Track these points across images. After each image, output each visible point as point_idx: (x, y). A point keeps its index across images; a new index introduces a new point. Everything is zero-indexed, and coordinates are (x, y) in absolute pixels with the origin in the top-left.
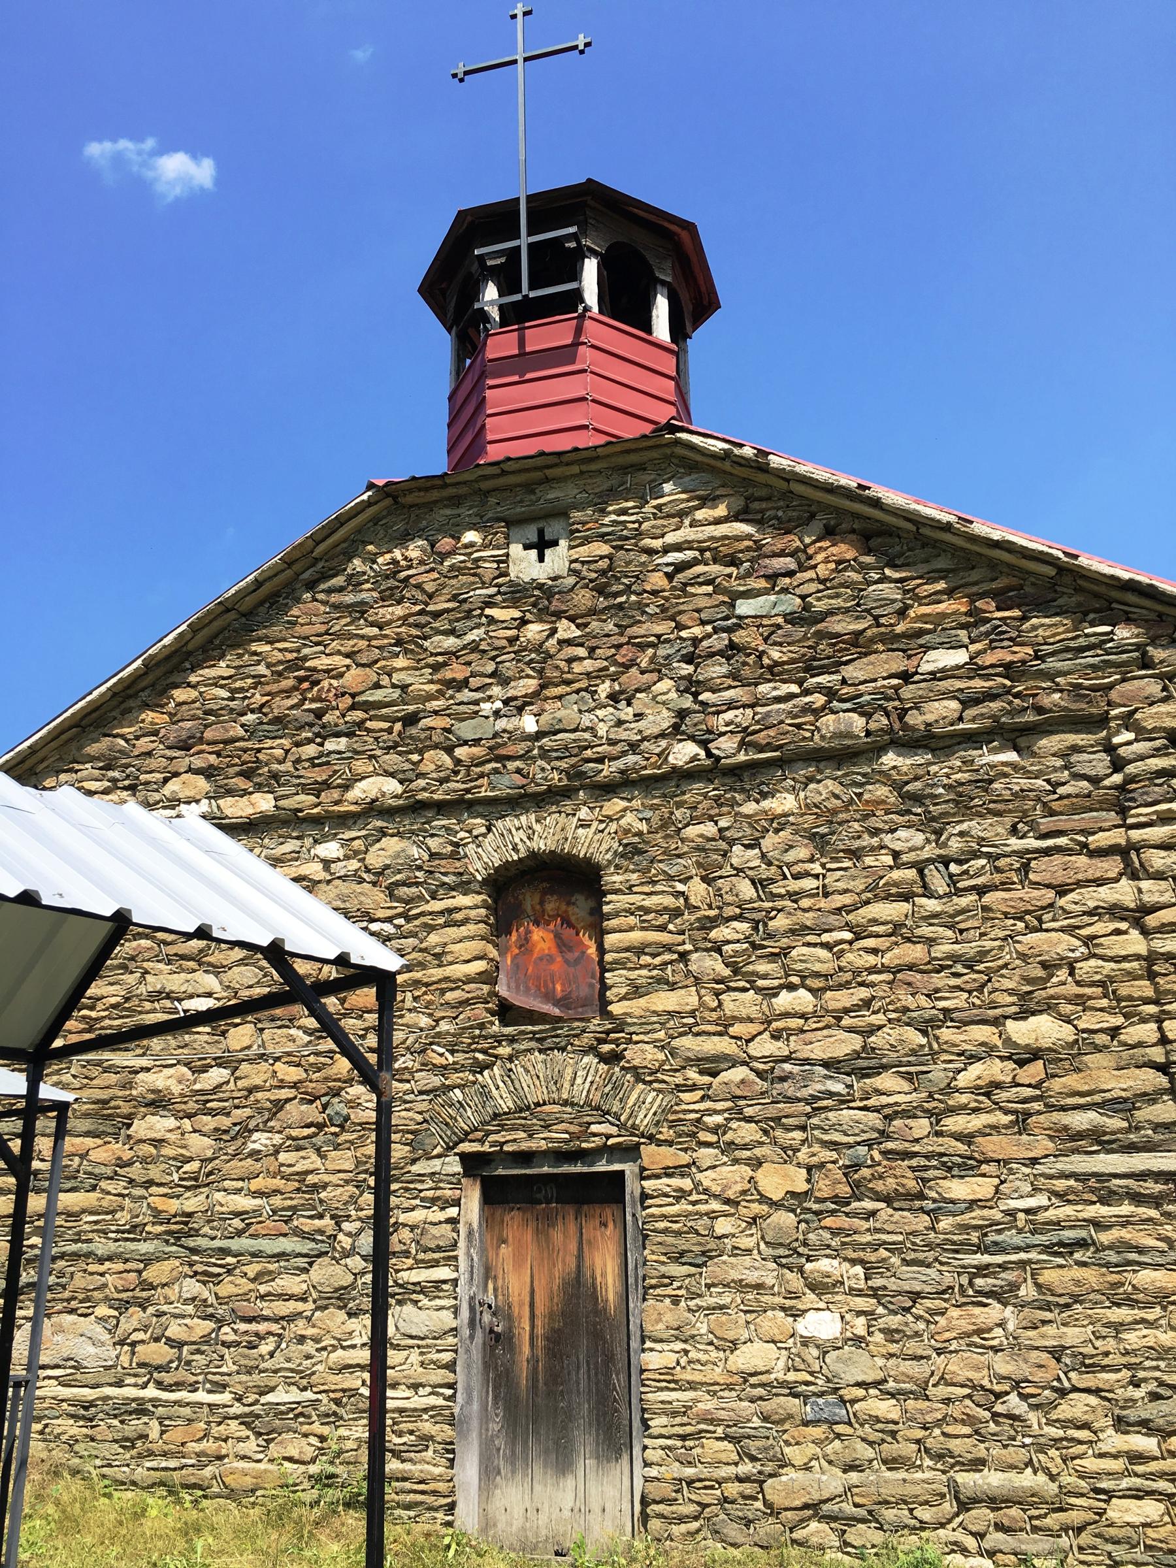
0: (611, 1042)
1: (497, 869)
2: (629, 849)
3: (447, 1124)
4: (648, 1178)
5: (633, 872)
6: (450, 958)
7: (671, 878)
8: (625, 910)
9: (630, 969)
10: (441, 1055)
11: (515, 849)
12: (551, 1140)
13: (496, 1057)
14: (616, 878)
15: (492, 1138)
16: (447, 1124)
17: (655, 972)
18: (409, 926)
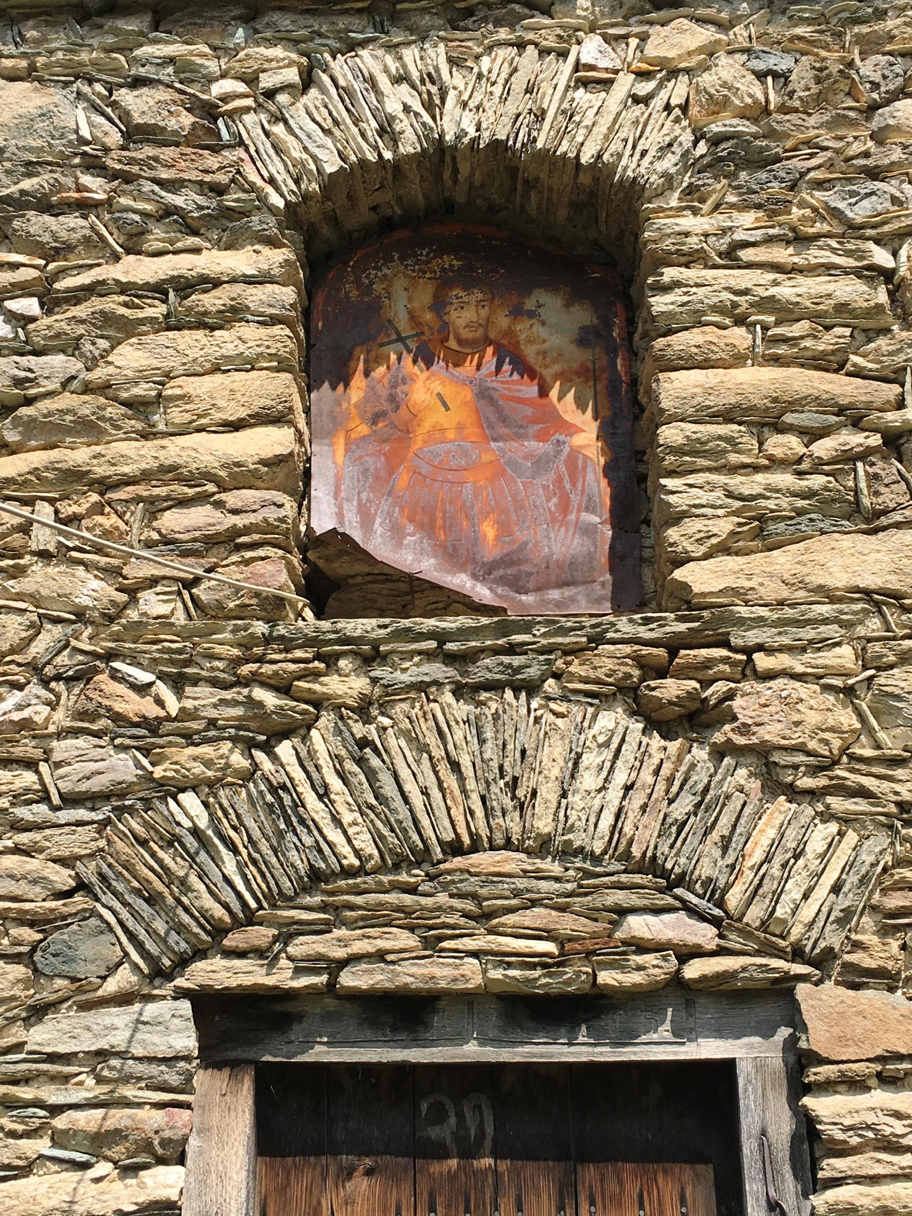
0: (683, 673)
1: (330, 184)
2: (724, 149)
3: (153, 899)
4: (827, 1087)
5: (743, 207)
6: (177, 415)
7: (854, 229)
8: (718, 309)
9: (734, 469)
10: (142, 689)
11: (387, 130)
12: (502, 958)
13: (319, 702)
14: (688, 222)
15: (303, 946)
16: (153, 899)
17: (817, 481)
18: (58, 321)
